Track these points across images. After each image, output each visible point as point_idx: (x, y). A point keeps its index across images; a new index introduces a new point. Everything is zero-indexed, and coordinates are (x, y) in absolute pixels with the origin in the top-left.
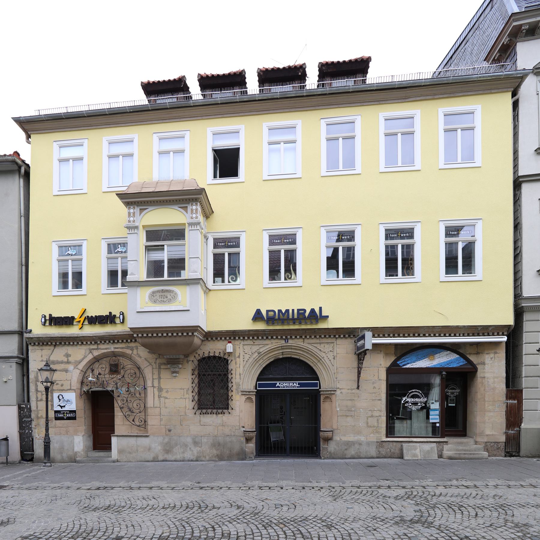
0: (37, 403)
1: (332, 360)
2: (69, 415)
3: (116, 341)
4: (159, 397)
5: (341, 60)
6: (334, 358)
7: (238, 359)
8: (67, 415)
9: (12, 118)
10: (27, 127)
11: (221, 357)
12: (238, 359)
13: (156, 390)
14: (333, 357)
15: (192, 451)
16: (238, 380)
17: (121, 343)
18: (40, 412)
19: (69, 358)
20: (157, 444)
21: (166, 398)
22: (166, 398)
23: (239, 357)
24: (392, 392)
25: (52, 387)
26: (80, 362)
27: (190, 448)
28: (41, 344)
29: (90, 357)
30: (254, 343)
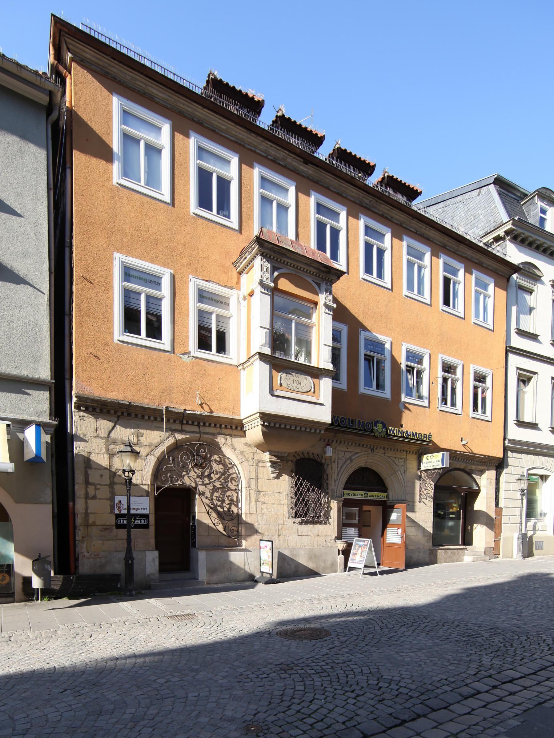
0: (86, 503)
1: (403, 474)
2: (139, 521)
3: (190, 422)
4: (257, 501)
5: (231, 85)
6: (404, 472)
7: (333, 463)
8: (136, 522)
9: (52, 15)
11: (299, 460)
13: (252, 492)
15: (290, 565)
16: (333, 487)
17: (191, 425)
18: (91, 515)
19: (140, 438)
20: (253, 560)
21: (264, 503)
22: (264, 503)
23: (334, 462)
25: (113, 479)
26: (157, 446)
28: (84, 409)
29: (170, 441)
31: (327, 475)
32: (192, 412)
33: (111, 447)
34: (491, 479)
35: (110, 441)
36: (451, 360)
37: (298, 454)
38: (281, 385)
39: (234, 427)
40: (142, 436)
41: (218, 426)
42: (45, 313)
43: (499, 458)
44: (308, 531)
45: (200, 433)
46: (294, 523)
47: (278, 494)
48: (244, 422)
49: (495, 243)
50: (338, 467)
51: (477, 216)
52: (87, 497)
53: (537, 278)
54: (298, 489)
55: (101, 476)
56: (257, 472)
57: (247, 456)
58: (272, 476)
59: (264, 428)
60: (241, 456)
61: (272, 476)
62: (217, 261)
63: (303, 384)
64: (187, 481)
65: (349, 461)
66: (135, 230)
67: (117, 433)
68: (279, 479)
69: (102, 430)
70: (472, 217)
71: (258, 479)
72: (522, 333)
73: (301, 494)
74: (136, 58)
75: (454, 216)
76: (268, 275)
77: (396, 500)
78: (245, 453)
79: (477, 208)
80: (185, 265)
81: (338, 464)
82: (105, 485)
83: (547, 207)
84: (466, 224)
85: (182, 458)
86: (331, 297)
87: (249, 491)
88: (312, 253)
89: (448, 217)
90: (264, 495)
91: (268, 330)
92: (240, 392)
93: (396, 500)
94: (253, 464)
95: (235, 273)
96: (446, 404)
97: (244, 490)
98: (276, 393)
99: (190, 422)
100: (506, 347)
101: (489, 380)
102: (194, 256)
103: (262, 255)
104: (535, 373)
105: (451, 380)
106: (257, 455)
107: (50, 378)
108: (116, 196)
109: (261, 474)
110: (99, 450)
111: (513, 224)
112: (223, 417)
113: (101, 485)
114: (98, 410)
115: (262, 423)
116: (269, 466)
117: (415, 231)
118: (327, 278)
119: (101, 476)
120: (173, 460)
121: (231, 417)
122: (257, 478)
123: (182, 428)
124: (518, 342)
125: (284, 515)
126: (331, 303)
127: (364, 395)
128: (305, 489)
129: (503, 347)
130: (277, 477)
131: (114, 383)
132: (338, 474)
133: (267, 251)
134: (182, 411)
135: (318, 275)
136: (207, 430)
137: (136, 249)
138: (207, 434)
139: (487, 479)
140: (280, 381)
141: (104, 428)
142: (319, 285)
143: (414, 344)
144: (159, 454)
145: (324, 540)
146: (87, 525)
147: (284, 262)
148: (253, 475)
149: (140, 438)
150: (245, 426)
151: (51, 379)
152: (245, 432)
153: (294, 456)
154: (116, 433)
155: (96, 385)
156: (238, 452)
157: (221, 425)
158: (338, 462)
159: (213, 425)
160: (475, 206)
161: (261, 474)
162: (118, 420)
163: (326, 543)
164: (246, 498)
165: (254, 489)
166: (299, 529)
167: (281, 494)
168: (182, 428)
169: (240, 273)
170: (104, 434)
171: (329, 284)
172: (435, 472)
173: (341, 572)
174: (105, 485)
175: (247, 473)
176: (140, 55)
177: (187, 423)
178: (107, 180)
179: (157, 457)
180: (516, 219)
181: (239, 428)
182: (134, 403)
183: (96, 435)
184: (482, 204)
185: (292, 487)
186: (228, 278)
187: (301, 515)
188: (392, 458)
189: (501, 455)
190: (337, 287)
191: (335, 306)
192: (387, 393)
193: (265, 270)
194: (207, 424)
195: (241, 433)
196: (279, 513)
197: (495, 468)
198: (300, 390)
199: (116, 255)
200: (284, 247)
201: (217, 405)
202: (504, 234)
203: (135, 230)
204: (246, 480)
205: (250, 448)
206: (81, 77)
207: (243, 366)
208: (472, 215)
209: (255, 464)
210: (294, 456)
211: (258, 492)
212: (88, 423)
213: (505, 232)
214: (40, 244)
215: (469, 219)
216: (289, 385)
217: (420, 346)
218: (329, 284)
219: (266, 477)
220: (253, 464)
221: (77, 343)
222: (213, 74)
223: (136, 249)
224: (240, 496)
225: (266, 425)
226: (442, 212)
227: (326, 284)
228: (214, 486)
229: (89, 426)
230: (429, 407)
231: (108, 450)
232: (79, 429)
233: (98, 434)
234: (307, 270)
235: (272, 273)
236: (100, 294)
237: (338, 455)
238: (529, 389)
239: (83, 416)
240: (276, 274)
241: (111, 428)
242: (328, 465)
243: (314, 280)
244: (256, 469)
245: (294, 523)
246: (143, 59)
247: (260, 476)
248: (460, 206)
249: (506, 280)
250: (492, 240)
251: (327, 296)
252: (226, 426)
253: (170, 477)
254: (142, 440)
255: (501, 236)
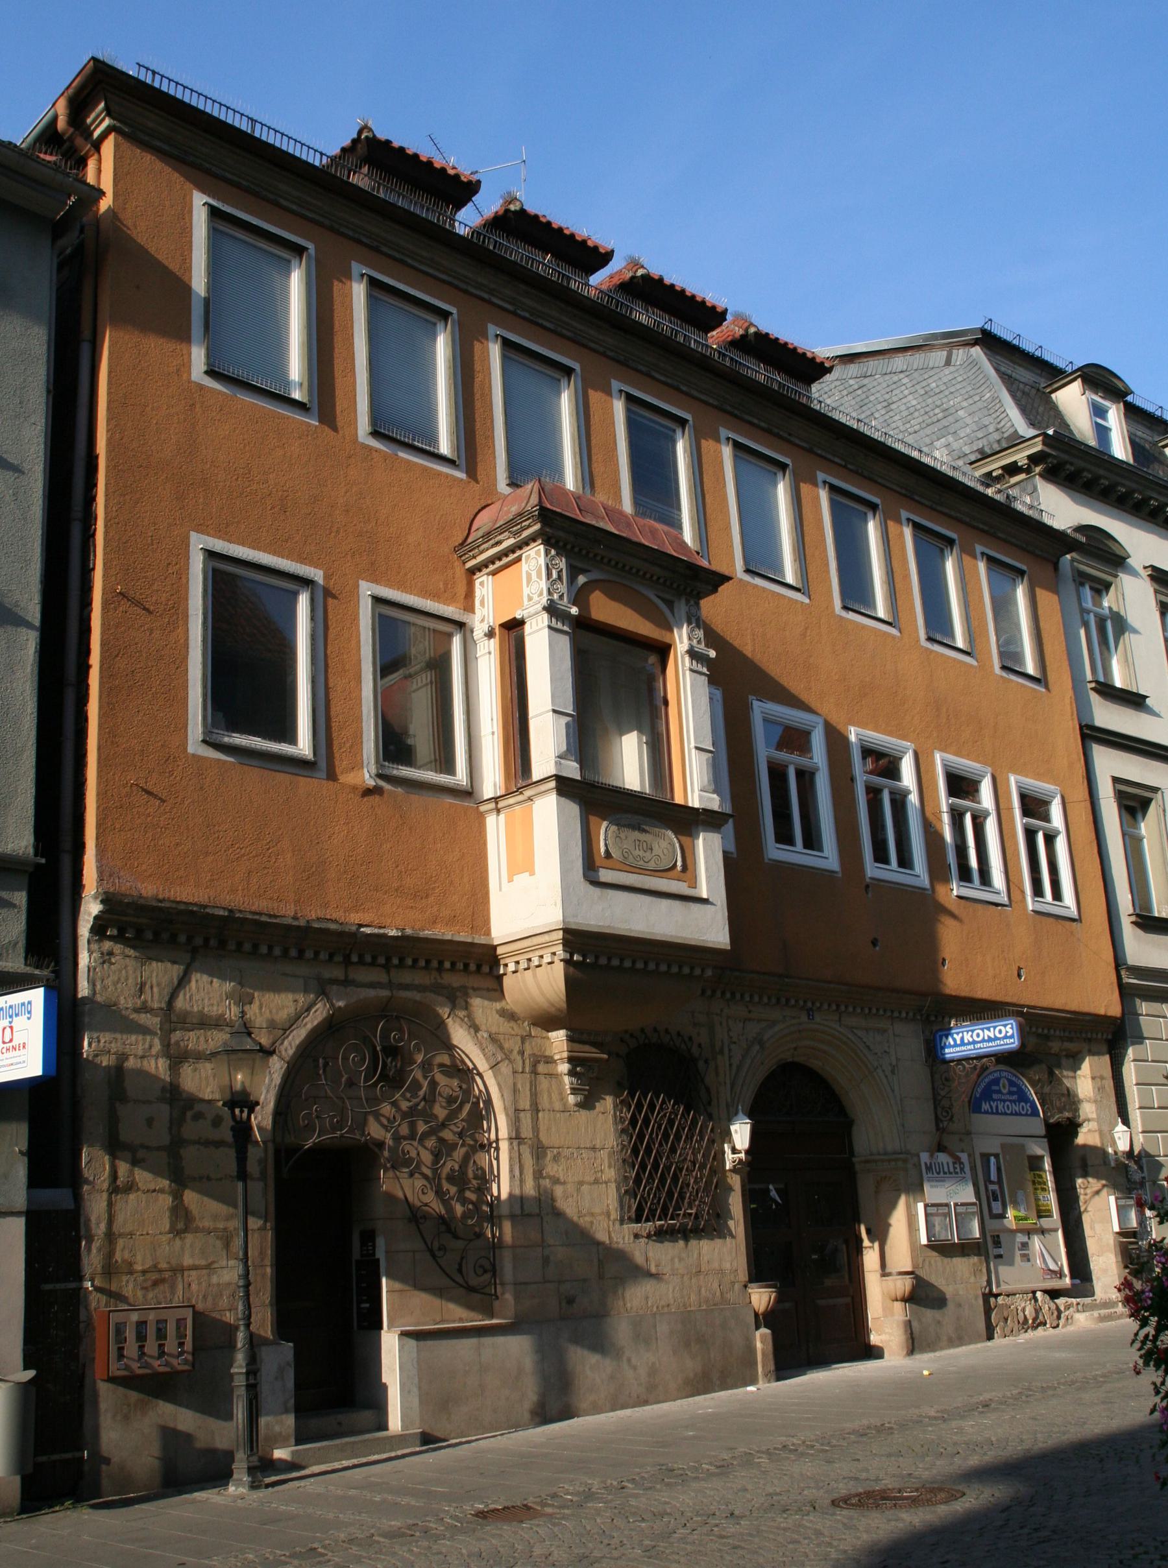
5: (396, 144)
6: (893, 1072)
10: (379, 294)
12: (719, 1057)
14: (890, 1069)
19: (247, 1008)
23: (721, 1052)
24: (68, 1456)
27: (629, 1360)
28: (115, 932)
29: (319, 1013)
30: (750, 1012)
31: (708, 1090)
32: (376, 931)
33: (176, 1036)
34: (1102, 1078)
35: (174, 1018)
36: (966, 765)
37: (632, 1035)
38: (608, 855)
39: (473, 967)
40: (251, 1003)
41: (435, 964)
42: (28, 683)
43: (1116, 1018)
44: (672, 1260)
45: (390, 985)
46: (636, 1236)
47: (592, 1154)
48: (500, 951)
49: (1007, 477)
50: (730, 1065)
51: (951, 411)
52: (115, 1189)
53: (1116, 560)
54: (641, 1136)
55: (150, 1122)
56: (534, 1095)
57: (506, 1046)
58: (572, 1099)
59: (571, 969)
60: (491, 1048)
61: (572, 1099)
62: (419, 544)
63: (657, 850)
64: (375, 1130)
65: (757, 1047)
66: (237, 480)
67: (191, 997)
68: (593, 1108)
69: (155, 990)
70: (937, 411)
71: (538, 1111)
72: (1107, 691)
73: (648, 1150)
74: (244, 126)
75: (891, 402)
76: (562, 588)
77: (895, 1153)
78: (501, 1037)
79: (947, 393)
80: (349, 557)
81: (730, 1057)
82: (158, 1149)
83: (1107, 403)
84: (924, 425)
85: (346, 1058)
86: (700, 633)
87: (516, 1148)
88: (651, 532)
89: (875, 402)
90: (556, 1159)
91: (569, 719)
92: (486, 871)
93: (879, 1154)
94: (524, 1067)
95: (460, 572)
96: (790, 841)
97: (504, 1146)
98: (605, 875)
99: (368, 959)
100: (1081, 728)
101: (1056, 811)
102: (368, 535)
103: (549, 542)
104: (1155, 790)
105: (891, 793)
106: (531, 1043)
107: (31, 851)
108: (198, 406)
109: (545, 1097)
110: (147, 1046)
111: (1044, 443)
112: (450, 942)
113: (148, 1148)
114: (149, 935)
115: (568, 956)
116: (566, 1072)
117: (843, 463)
118: (688, 590)
119: (150, 1122)
120: (326, 1065)
121: (469, 940)
122: (536, 1109)
123: (346, 976)
124: (1107, 716)
125: (608, 1215)
126: (702, 646)
127: (779, 865)
128: (657, 1135)
129: (1074, 728)
130: (587, 1104)
131: (187, 860)
132: (733, 1085)
133: (561, 534)
134: (354, 928)
135: (668, 583)
136: (407, 977)
137: (238, 522)
138: (407, 987)
139: (1093, 1078)
140: (606, 845)
141: (159, 985)
142: (670, 604)
143: (876, 730)
144: (291, 1052)
145: (716, 1285)
146: (110, 1269)
147: (596, 555)
148: (525, 1103)
149: (247, 1008)
150: (502, 962)
151: (36, 855)
152: (500, 978)
153: (622, 1040)
154: (188, 997)
155: (144, 867)
156: (486, 1035)
157: (441, 963)
158: (730, 1050)
159: (422, 963)
160: (943, 388)
161: (545, 1097)
162: (193, 959)
163: (722, 1294)
164: (511, 1171)
165: (530, 1142)
166: (650, 1254)
167: (598, 1154)
168: (346, 976)
169: (473, 571)
170: (156, 999)
171: (692, 602)
172: (975, 1067)
173: (769, 1382)
174: (158, 1149)
175: (508, 1094)
176: (252, 120)
177: (361, 962)
178: (178, 370)
179: (287, 1059)
180: (1051, 432)
181: (486, 969)
182: (240, 911)
183: (139, 1003)
184: (958, 386)
185: (623, 1131)
186: (446, 584)
187: (652, 1213)
188: (859, 1033)
189: (1115, 1010)
190: (709, 606)
191: (712, 654)
192: (829, 857)
193: (555, 575)
194: (409, 962)
195: (491, 983)
196: (597, 1210)
197: (1105, 1048)
198: (652, 865)
199: (194, 536)
200: (594, 523)
201: (435, 908)
202: (1026, 462)
203: (237, 480)
204: (507, 1115)
205: (512, 1024)
206: (128, 161)
207: (497, 803)
208: (938, 407)
209: (527, 1070)
210: (622, 1040)
211: (539, 1151)
212: (120, 971)
213: (1029, 457)
214: (25, 519)
215: (931, 414)
216: (626, 855)
217: (890, 734)
218: (692, 602)
219: (558, 1106)
220: (524, 1067)
221: (103, 757)
222: (370, 130)
223: (238, 522)
224: (495, 1162)
225: (577, 962)
226: (856, 387)
227: (688, 602)
228: (442, 1140)
229: (123, 980)
230: (1010, 905)
231: (169, 1045)
232: (98, 987)
233: (145, 1002)
234: (645, 574)
235: (572, 579)
236: (157, 634)
237: (729, 1030)
238: (1147, 828)
239: (111, 953)
240: (582, 579)
241: (176, 982)
242: (706, 1061)
243: (661, 594)
244: (531, 1082)
245: (636, 1236)
246: (258, 126)
247: (544, 1102)
248: (905, 381)
249: (1051, 568)
250: (1000, 472)
251: (692, 631)
252: (453, 964)
253: (317, 1117)
254: (252, 1011)
255: (1019, 464)
